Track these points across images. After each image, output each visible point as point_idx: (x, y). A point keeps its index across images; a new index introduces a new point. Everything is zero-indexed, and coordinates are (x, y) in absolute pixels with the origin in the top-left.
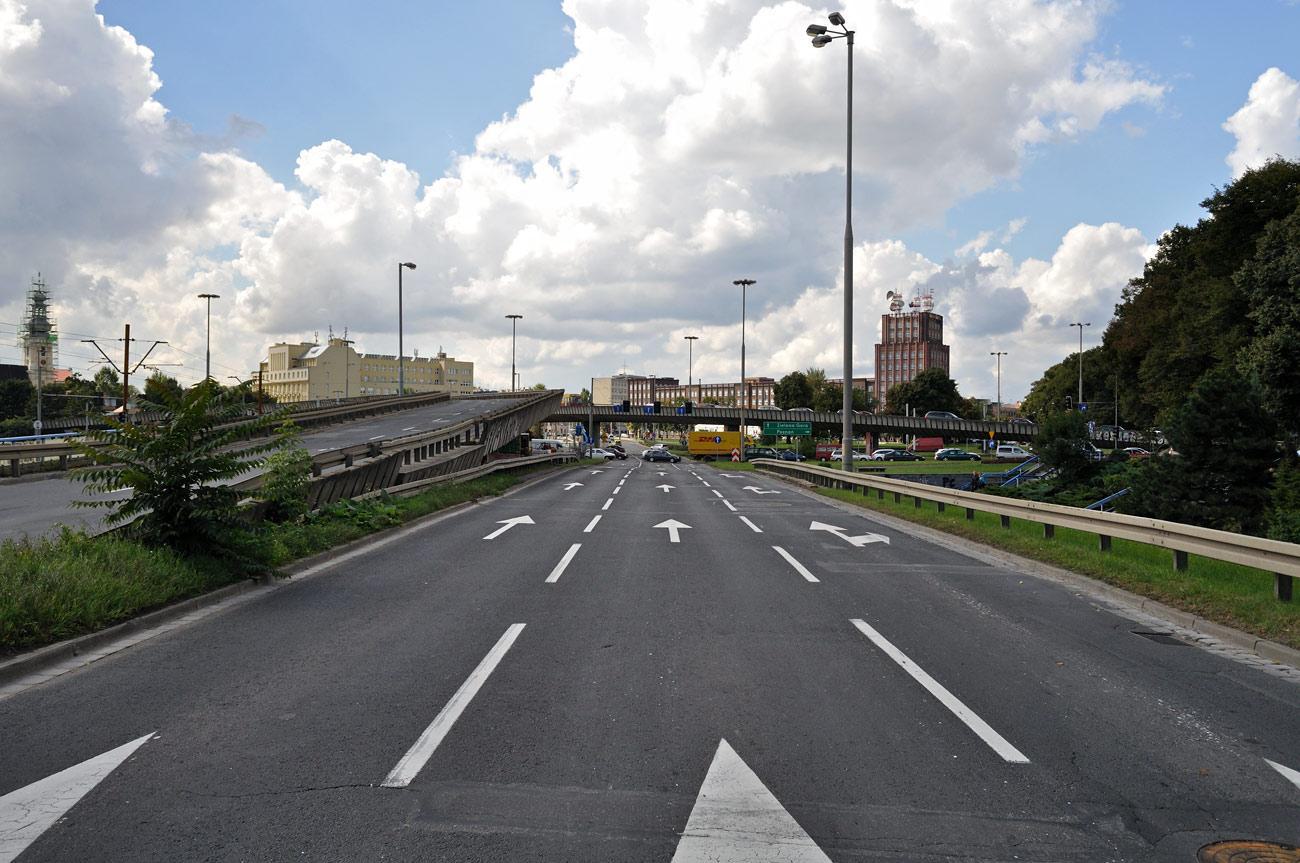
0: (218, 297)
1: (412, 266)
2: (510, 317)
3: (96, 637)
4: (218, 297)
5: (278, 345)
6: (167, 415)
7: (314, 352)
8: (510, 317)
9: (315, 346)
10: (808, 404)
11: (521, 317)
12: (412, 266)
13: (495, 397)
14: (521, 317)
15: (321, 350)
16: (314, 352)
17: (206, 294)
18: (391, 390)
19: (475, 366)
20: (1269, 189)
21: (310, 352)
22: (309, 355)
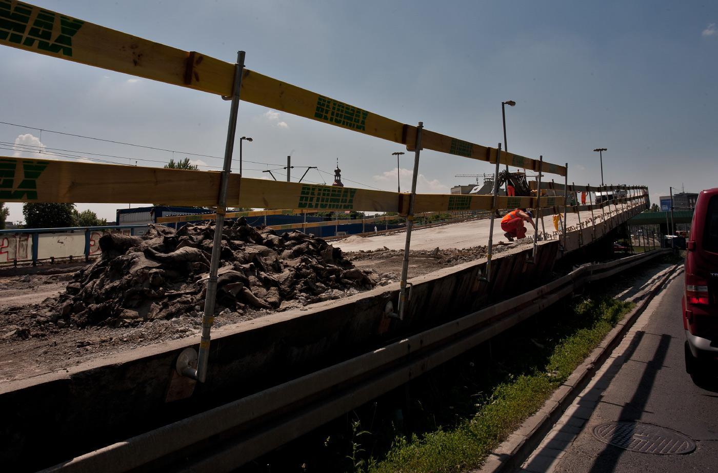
0: (404, 153)
1: (512, 103)
2: (597, 150)
3: (604, 197)
4: (404, 153)
5: (456, 187)
6: (237, 242)
7: (475, 190)
8: (597, 150)
9: (477, 186)
10: (692, 210)
11: (606, 150)
12: (512, 103)
13: (686, 335)
14: (606, 150)
15: (479, 188)
16: (475, 190)
17: (397, 152)
18: (141, 219)
19: (672, 340)
20: (126, 341)
21: (473, 189)
22: (473, 191)
